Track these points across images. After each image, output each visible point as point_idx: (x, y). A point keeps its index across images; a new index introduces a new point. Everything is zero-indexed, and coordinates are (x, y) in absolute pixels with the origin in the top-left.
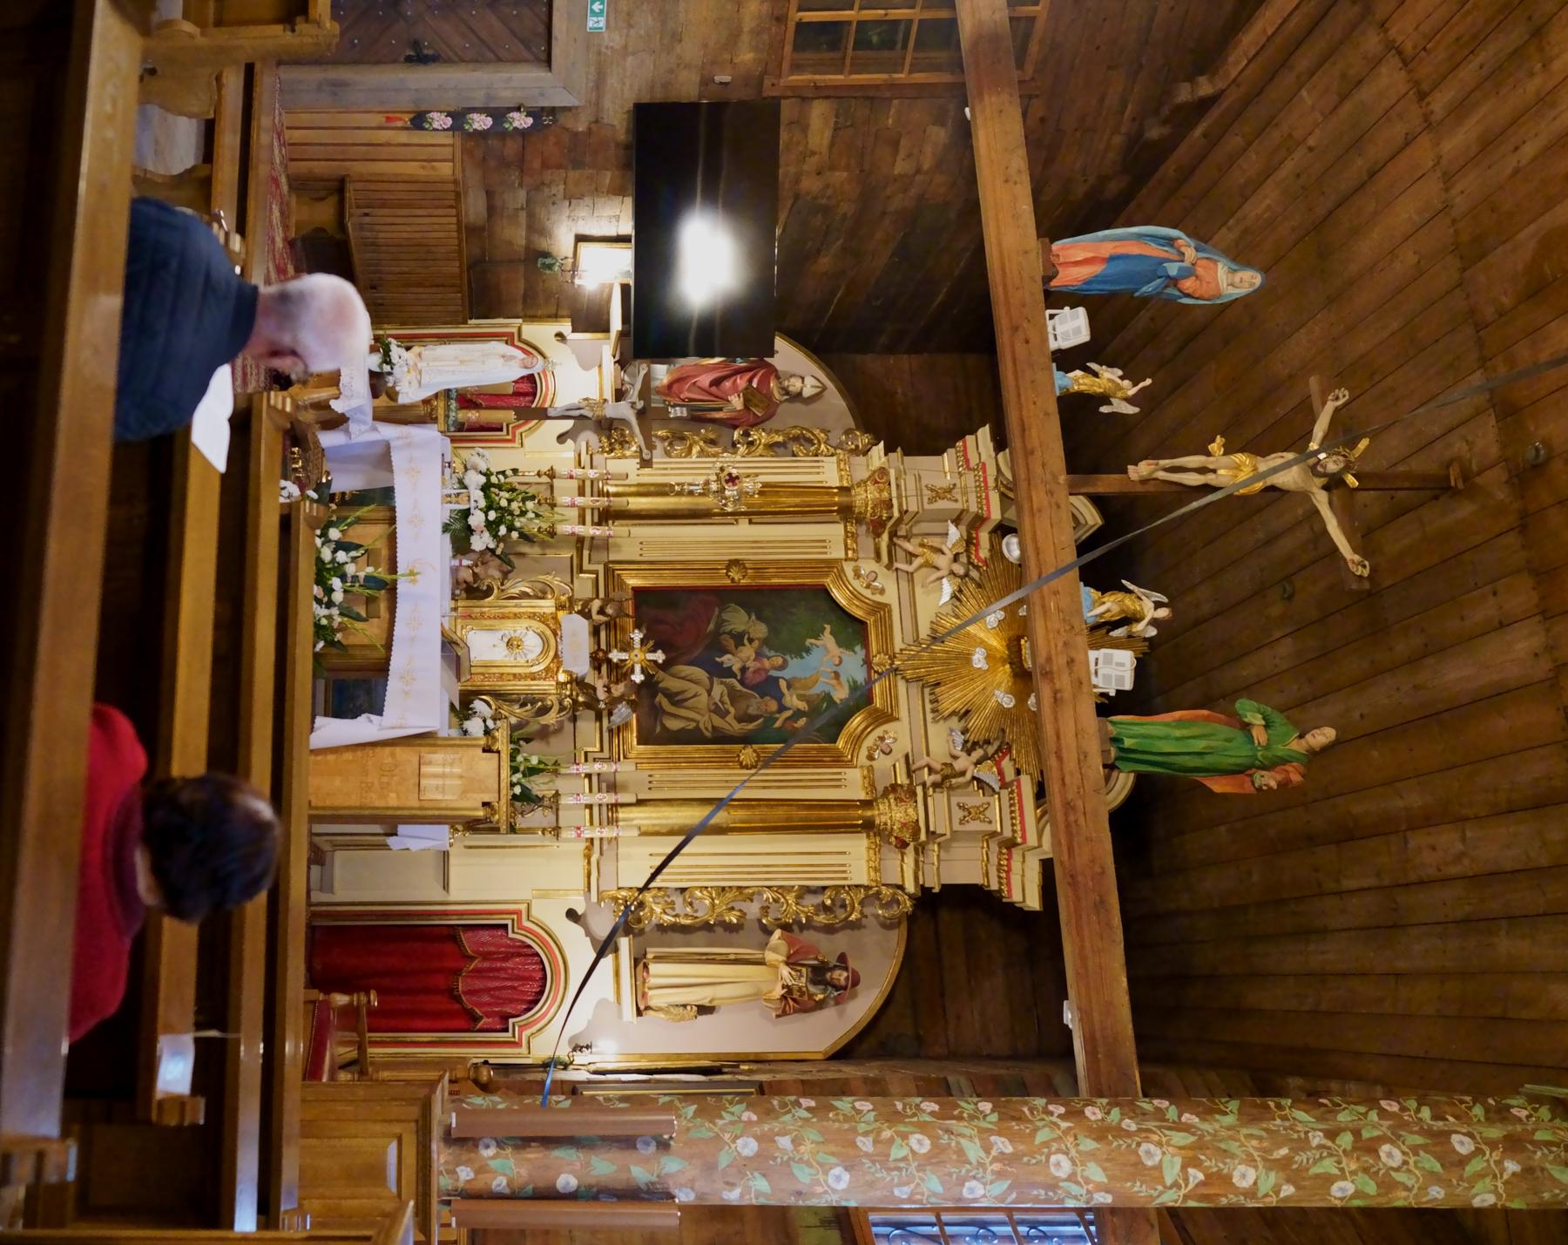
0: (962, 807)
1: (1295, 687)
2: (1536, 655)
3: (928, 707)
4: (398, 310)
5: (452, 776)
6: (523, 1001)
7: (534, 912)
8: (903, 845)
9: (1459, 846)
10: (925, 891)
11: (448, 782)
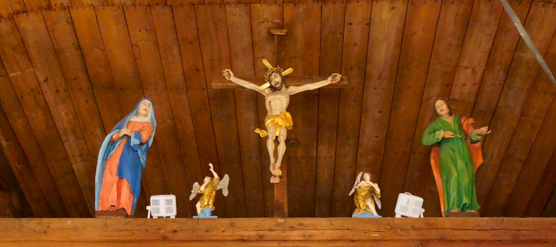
1: (347, 148)
2: (393, 8)
9: (469, 71)
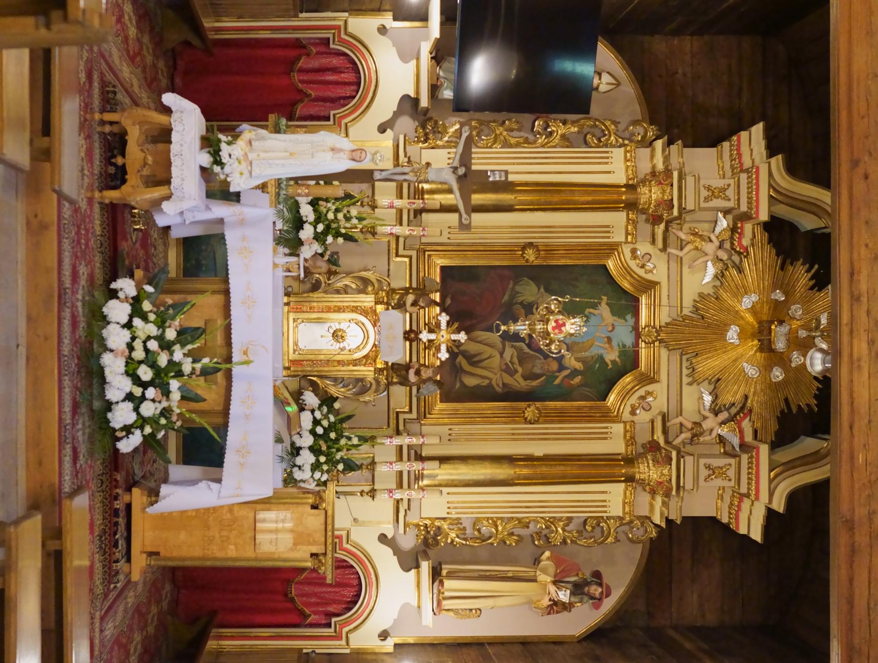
0: (708, 467)
3: (685, 372)
4: (225, 115)
5: (284, 530)
6: (339, 602)
7: (353, 537)
8: (653, 493)
10: (669, 522)
11: (280, 536)
